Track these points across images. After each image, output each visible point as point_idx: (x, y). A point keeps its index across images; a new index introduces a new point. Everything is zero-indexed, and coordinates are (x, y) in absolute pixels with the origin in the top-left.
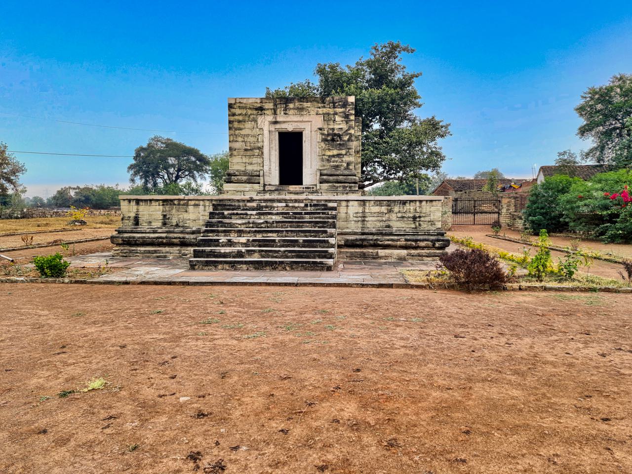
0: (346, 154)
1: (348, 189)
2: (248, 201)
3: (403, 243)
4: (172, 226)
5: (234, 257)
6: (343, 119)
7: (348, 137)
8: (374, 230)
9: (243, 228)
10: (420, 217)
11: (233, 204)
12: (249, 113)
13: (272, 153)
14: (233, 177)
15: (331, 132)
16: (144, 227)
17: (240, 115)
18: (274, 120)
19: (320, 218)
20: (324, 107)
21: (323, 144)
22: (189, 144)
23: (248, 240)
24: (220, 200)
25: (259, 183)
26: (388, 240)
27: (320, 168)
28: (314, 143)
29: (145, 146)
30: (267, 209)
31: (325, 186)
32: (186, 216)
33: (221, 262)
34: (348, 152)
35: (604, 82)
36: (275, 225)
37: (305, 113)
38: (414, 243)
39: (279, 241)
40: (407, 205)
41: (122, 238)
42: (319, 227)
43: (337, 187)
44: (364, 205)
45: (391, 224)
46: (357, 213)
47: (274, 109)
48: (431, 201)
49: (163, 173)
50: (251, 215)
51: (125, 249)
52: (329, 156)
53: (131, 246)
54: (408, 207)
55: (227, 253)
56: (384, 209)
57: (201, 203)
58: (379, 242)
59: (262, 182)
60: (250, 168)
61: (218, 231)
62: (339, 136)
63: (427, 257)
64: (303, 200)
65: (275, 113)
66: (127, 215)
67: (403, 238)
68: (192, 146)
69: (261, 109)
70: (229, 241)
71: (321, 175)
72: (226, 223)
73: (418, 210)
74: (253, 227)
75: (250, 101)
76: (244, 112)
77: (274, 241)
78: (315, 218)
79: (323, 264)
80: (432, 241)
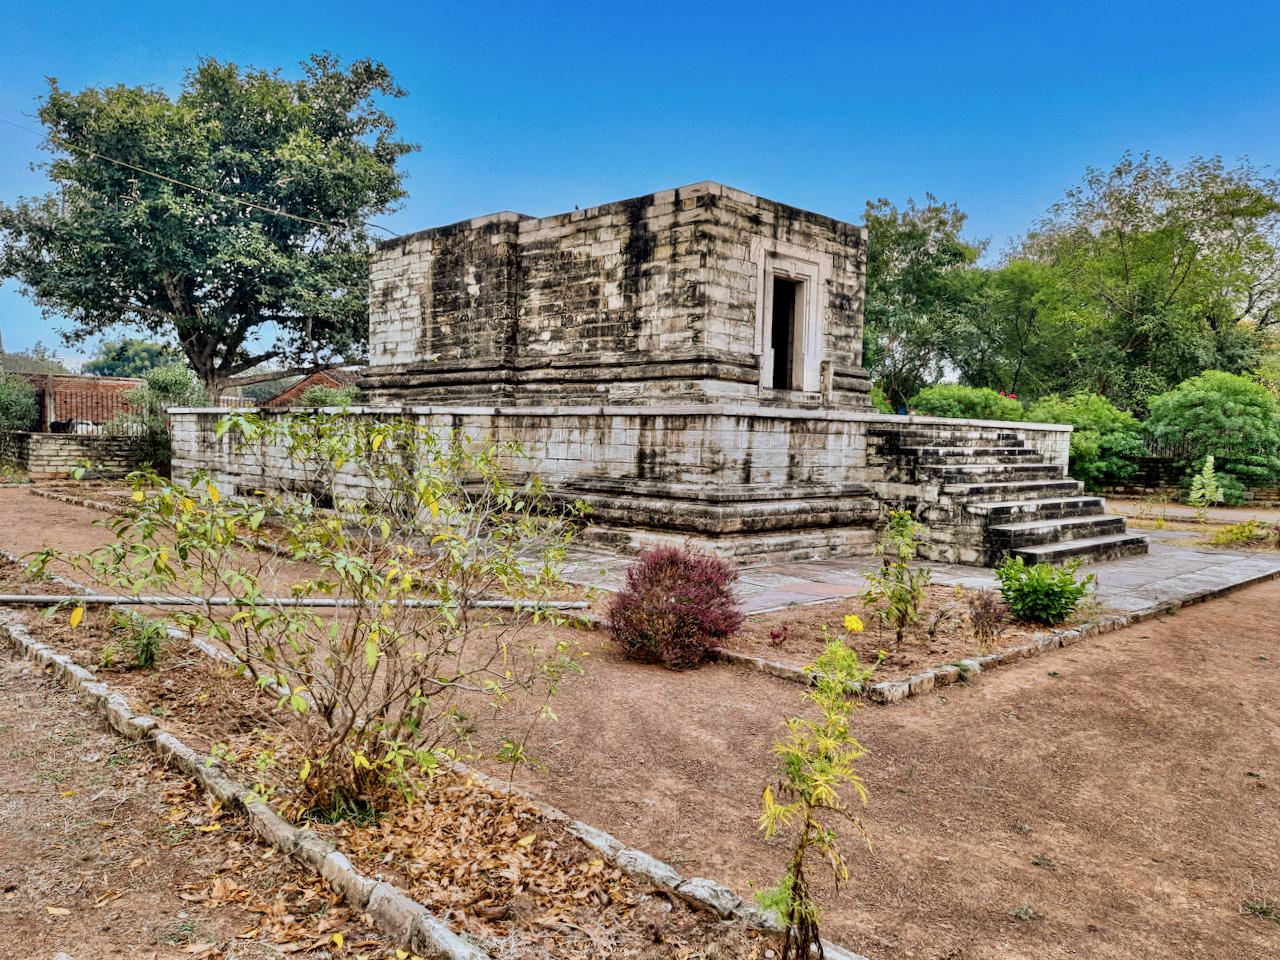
4: (802, 481)
12: (740, 226)
17: (726, 225)
18: (772, 249)
28: (821, 308)
51: (742, 546)
52: (836, 337)
57: (544, 422)
69: (756, 220)
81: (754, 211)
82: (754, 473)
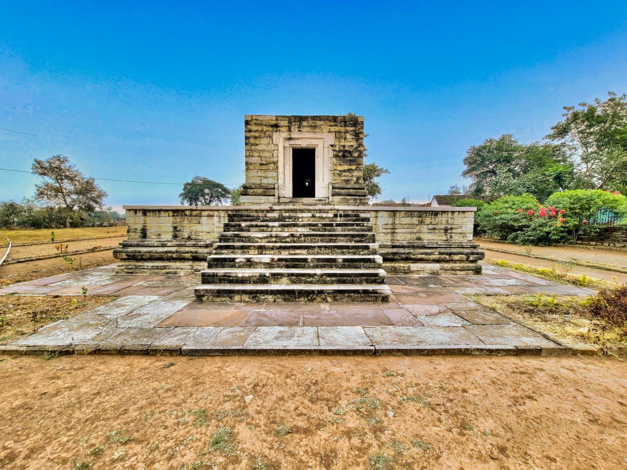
0: (356, 170)
1: (358, 201)
2: (268, 211)
3: (436, 257)
5: (255, 283)
6: (354, 137)
7: (357, 154)
8: (404, 242)
9: (263, 243)
10: (451, 229)
11: (252, 214)
12: (265, 130)
13: (286, 168)
14: (249, 190)
15: (342, 148)
16: (152, 239)
17: (256, 131)
19: (353, 230)
20: (336, 125)
21: (334, 160)
22: (218, 181)
23: (273, 259)
24: (236, 211)
25: (274, 196)
26: (422, 254)
27: (333, 182)
28: (327, 158)
29: (190, 182)
30: (290, 220)
31: (337, 198)
32: (198, 228)
33: (238, 292)
34: (358, 167)
35: (479, 144)
36: (303, 239)
37: (317, 130)
38: (447, 257)
39: (313, 260)
40: (439, 216)
41: (126, 252)
42: (356, 242)
43: (348, 200)
44: (395, 216)
45: (422, 236)
46: (387, 224)
47: (289, 126)
48: (464, 212)
49: (201, 198)
50: (273, 227)
51: (130, 265)
52: (340, 171)
53: (137, 262)
54: (440, 219)
55: (245, 277)
56: (415, 220)
57: (216, 213)
58: (411, 256)
59: (276, 195)
60: (265, 181)
61: (233, 247)
62: (350, 152)
63: (461, 270)
64: (328, 210)
65: (290, 130)
66: (133, 227)
67: (436, 252)
68: (219, 182)
69: (276, 126)
70: (249, 260)
71: (333, 188)
72: (243, 237)
73: (450, 222)
74: (276, 242)
75: (266, 118)
76: (260, 128)
77: (305, 260)
78: (349, 230)
79: (376, 293)
80: (467, 254)
81: (274, 122)
82: (148, 234)
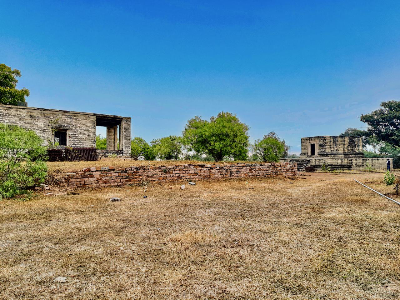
56: (319, 160)
62: (322, 144)
71: (318, 153)
